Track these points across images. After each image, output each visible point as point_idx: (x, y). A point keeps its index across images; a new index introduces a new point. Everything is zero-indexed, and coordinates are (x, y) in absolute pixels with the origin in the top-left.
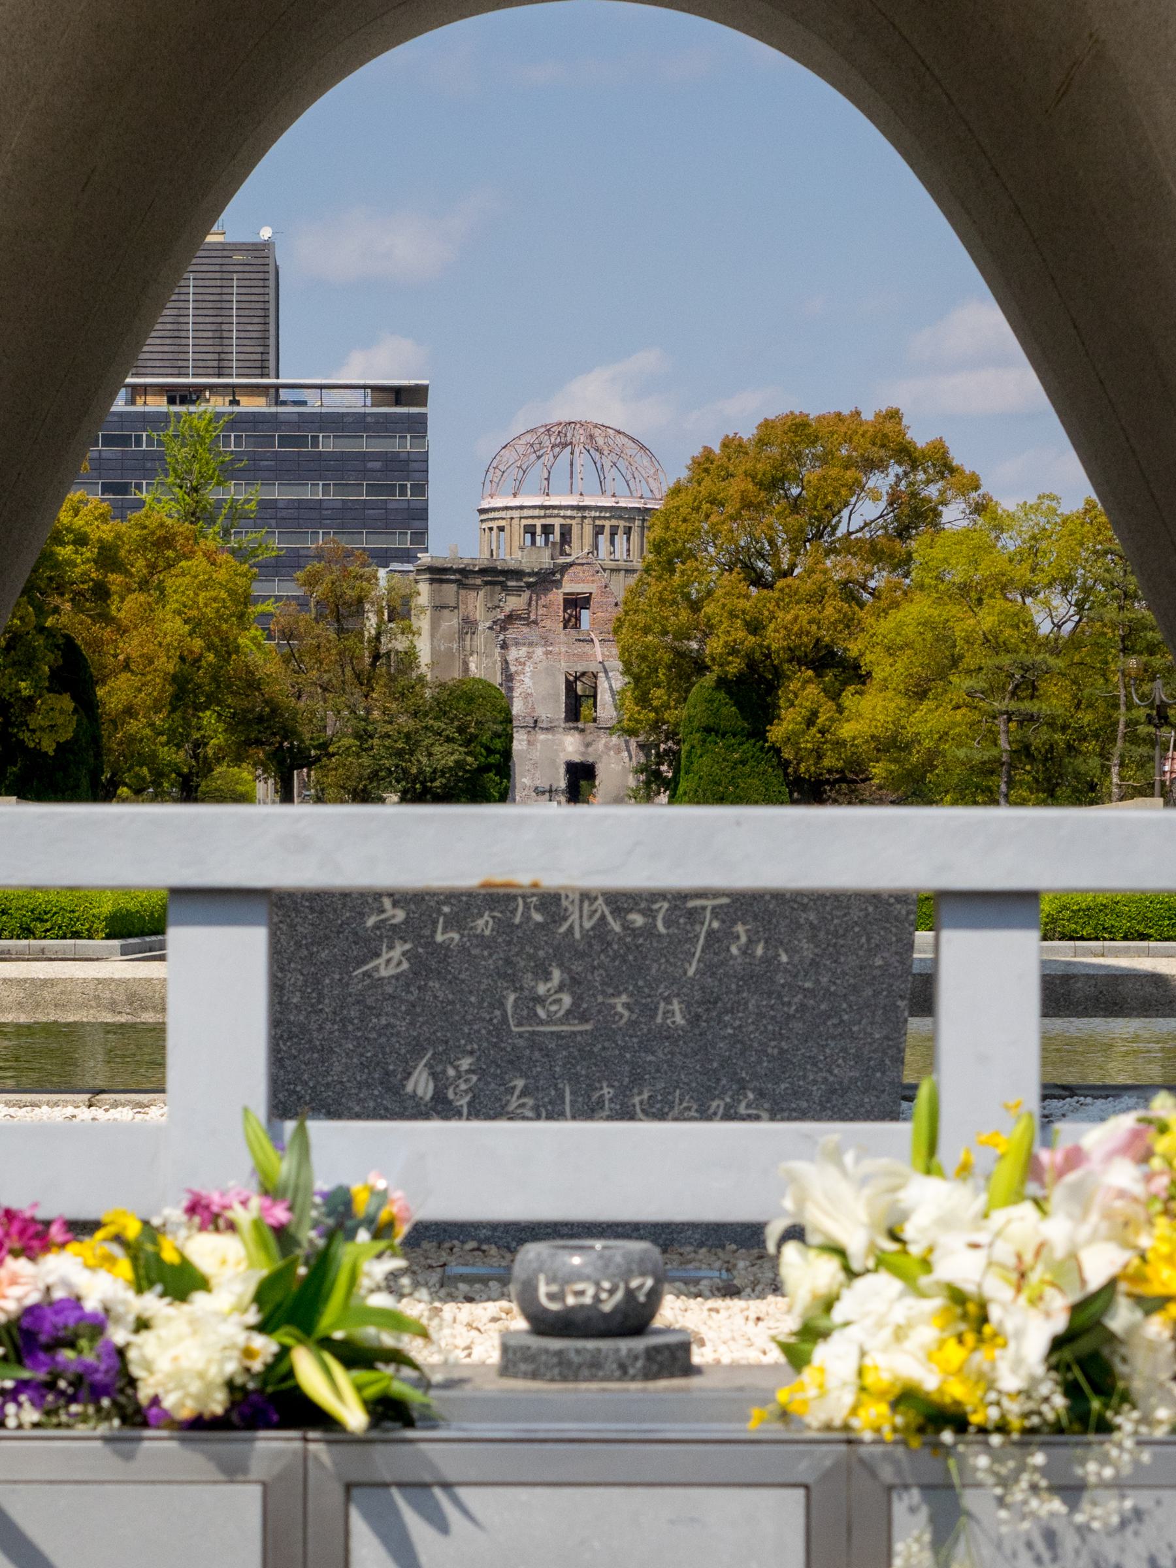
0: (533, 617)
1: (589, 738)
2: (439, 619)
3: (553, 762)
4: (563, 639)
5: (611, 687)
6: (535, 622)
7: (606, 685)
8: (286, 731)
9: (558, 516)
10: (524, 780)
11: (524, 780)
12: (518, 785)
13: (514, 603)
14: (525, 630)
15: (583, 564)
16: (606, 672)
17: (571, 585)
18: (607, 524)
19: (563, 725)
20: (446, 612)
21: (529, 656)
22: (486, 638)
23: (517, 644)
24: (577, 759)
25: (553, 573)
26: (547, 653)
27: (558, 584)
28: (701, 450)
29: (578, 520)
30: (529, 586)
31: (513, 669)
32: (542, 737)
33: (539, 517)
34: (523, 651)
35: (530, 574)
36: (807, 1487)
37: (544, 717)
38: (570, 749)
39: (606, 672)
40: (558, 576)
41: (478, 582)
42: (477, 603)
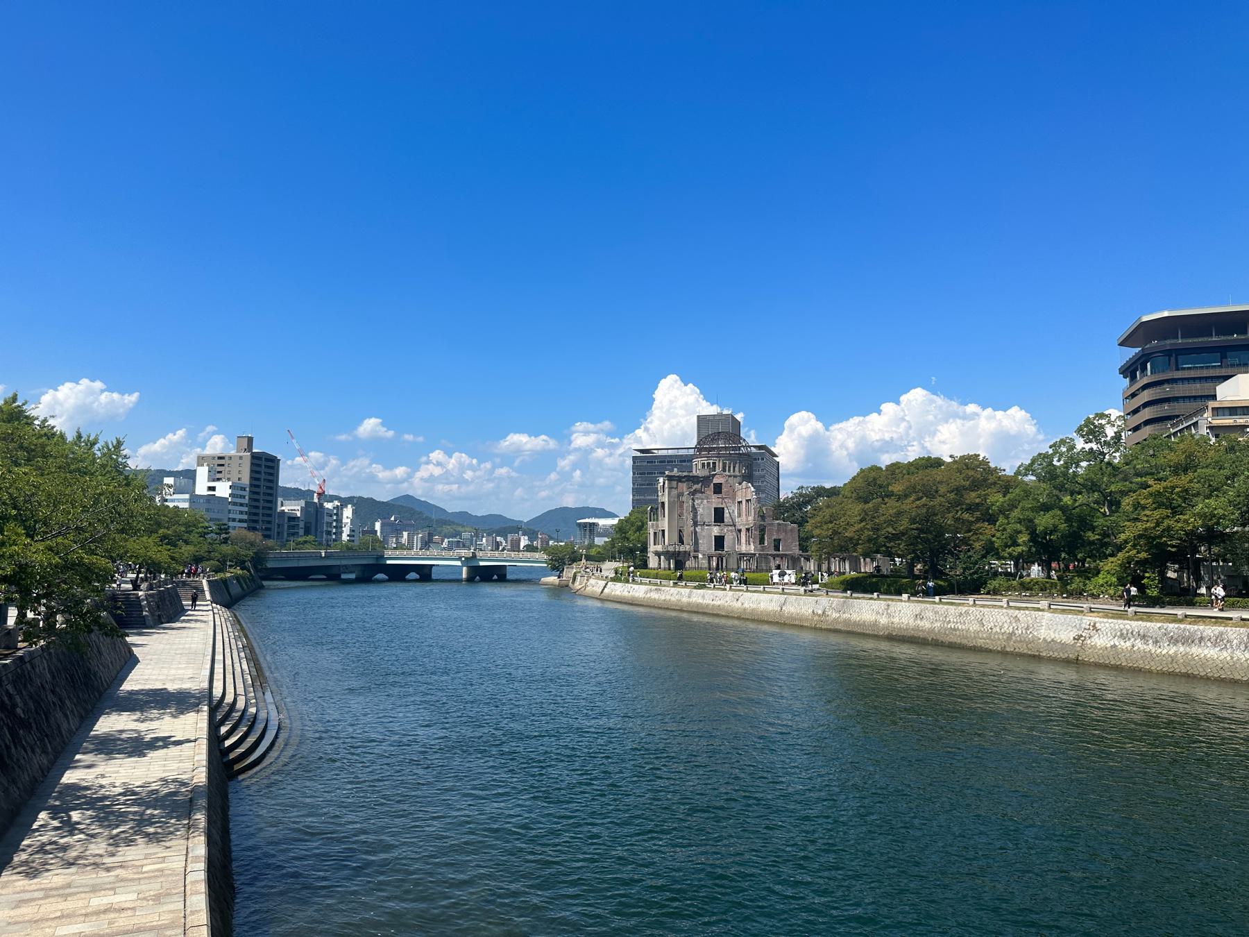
13: (698, 486)
42: (683, 487)
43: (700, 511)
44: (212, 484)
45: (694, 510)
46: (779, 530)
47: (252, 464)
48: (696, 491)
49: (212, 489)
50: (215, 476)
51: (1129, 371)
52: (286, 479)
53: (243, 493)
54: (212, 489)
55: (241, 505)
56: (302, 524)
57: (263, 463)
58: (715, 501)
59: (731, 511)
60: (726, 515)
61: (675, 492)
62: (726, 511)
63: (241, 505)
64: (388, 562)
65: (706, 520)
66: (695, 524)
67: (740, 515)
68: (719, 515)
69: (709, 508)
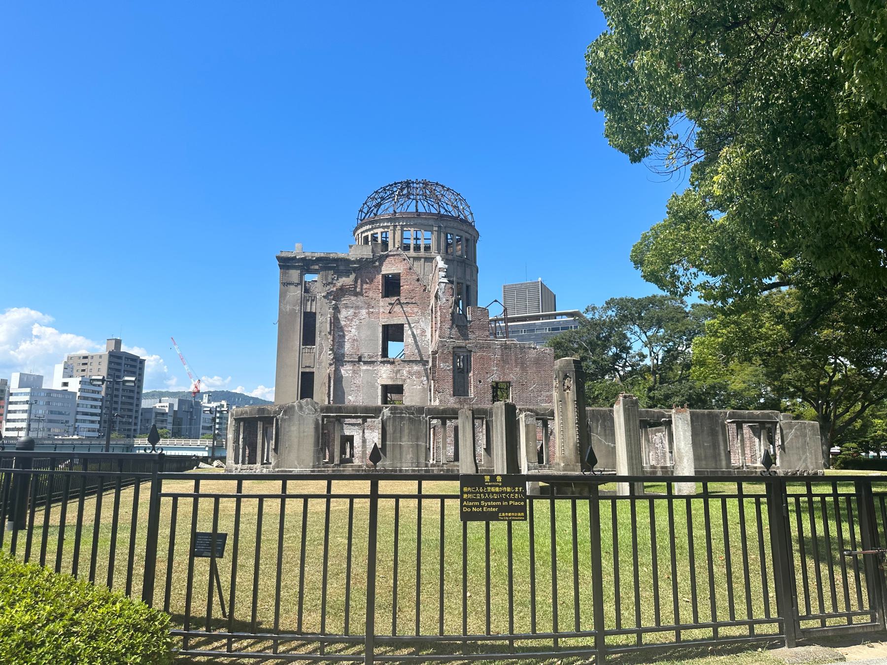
0: (358, 290)
1: (398, 367)
2: (286, 291)
3: (373, 386)
4: (383, 304)
5: (413, 333)
6: (361, 294)
7: (410, 332)
8: (867, 51)
10: (350, 397)
11: (350, 397)
13: (346, 281)
14: (353, 298)
15: (393, 255)
16: (409, 324)
17: (389, 268)
18: (369, 233)
19: (380, 359)
20: (292, 287)
22: (322, 305)
23: (346, 307)
24: (390, 382)
26: (368, 313)
27: (378, 269)
29: (391, 228)
30: (355, 270)
31: (343, 323)
32: (364, 367)
33: (369, 230)
34: (351, 312)
35: (354, 262)
36: (496, 301)
37: (366, 355)
38: (384, 376)
39: (409, 324)
40: (377, 263)
41: (317, 267)
43: (351, 333)
44: (66, 380)
45: (336, 328)
48: (342, 292)
49: (65, 384)
50: (68, 371)
55: (95, 400)
56: (170, 420)
58: (384, 312)
63: (95, 400)
65: (366, 353)
66: (339, 360)
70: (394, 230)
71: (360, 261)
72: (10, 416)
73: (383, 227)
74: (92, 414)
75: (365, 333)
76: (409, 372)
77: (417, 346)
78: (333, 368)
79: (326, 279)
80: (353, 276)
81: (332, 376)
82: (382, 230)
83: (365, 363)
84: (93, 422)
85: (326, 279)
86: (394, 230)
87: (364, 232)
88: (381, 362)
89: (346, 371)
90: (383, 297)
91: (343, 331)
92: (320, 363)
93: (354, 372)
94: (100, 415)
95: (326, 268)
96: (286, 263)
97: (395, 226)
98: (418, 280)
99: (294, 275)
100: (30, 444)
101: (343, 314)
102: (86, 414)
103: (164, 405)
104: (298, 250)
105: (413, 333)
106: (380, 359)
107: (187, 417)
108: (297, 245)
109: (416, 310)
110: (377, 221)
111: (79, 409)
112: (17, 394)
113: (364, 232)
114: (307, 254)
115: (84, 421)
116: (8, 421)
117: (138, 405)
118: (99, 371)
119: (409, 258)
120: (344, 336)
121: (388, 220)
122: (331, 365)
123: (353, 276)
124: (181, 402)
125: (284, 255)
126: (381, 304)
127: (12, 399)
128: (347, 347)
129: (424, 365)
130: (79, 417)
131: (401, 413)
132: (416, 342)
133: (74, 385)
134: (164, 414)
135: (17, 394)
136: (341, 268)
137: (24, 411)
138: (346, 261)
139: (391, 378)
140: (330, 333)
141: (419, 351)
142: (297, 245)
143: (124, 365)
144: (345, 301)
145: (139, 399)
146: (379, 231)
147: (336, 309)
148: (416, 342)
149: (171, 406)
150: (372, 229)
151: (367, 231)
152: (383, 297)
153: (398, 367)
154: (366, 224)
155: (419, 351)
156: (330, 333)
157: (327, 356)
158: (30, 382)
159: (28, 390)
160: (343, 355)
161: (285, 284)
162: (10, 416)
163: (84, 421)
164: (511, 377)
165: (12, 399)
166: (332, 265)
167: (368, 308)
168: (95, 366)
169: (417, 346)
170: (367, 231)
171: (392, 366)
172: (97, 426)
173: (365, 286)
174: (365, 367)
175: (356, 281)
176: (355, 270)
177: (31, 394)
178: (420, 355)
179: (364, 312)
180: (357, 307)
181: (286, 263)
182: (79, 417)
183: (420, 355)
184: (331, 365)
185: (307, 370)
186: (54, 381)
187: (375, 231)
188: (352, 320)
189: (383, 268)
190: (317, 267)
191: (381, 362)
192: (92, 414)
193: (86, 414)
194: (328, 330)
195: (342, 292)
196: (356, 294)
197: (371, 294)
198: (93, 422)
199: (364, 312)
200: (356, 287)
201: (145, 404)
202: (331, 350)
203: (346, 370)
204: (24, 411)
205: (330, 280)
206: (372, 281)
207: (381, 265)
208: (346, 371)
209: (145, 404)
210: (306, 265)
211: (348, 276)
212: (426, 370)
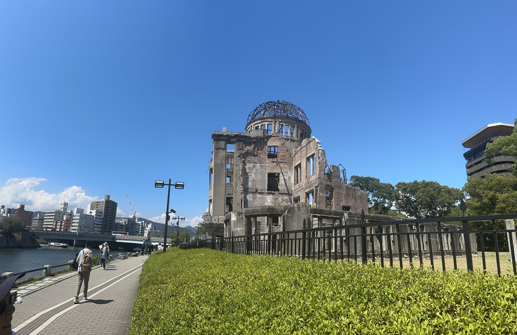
0: (256, 153)
5: (284, 178)
6: (257, 155)
7: (283, 178)
9: (266, 121)
12: (245, 226)
13: (250, 148)
14: (253, 158)
15: (275, 136)
16: (282, 173)
18: (260, 125)
19: (266, 192)
20: (221, 150)
21: (254, 167)
22: (237, 160)
23: (249, 162)
25: (264, 139)
26: (261, 166)
28: (422, 181)
29: (273, 122)
30: (254, 142)
31: (247, 171)
33: (260, 123)
34: (252, 165)
35: (253, 138)
37: (259, 189)
38: (269, 201)
39: (282, 173)
40: (266, 140)
41: (234, 140)
42: (231, 148)
43: (252, 176)
44: (91, 211)
45: (245, 175)
46: (347, 195)
47: (106, 204)
48: (247, 154)
49: (91, 213)
50: (92, 208)
51: (467, 156)
52: (119, 212)
53: (101, 214)
54: (91, 213)
55: (100, 219)
56: (125, 228)
57: (110, 204)
58: (270, 166)
59: (287, 178)
60: (282, 182)
61: (222, 153)
62: (281, 178)
63: (100, 219)
64: (117, 241)
65: (259, 187)
66: (246, 191)
67: (297, 181)
68: (273, 181)
69: (263, 174)
70: (275, 123)
71: (257, 138)
72: (73, 224)
73: (269, 121)
74: (99, 225)
75: (259, 177)
76: (282, 199)
77: (286, 185)
78: (243, 195)
79: (239, 147)
80: (253, 146)
81: (243, 200)
82: (268, 123)
83: (259, 193)
84: (99, 228)
85: (239, 147)
86: (275, 123)
87: (256, 124)
88: (267, 193)
89: (249, 197)
90: (268, 158)
91: (247, 175)
92: (236, 193)
93: (254, 198)
94: (101, 225)
95: (238, 141)
96: (217, 138)
97: (276, 121)
98: (287, 151)
99: (222, 144)
100: (80, 235)
101: (248, 166)
102: (97, 224)
103: (122, 222)
104: (224, 131)
105: (284, 178)
106: (266, 192)
107: (131, 227)
108: (223, 128)
109: (286, 166)
110: (265, 118)
111: (95, 222)
112: (76, 216)
113: (256, 124)
114: (229, 133)
115: (96, 227)
116: (72, 226)
117: (114, 221)
118: (102, 208)
119: (283, 139)
120: (248, 178)
121: (271, 118)
122: (242, 193)
123: (253, 146)
124: (127, 220)
125: (216, 133)
126: (267, 161)
127: (74, 218)
128: (250, 183)
129: (289, 196)
130: (95, 226)
131: (354, 217)
132: (286, 183)
133: (94, 213)
134: (123, 225)
135: (76, 216)
136: (247, 141)
137: (77, 223)
138: (249, 138)
139: (272, 202)
140: (242, 176)
141: (287, 188)
142: (223, 128)
143: (111, 206)
144: (248, 159)
145: (115, 219)
146: (266, 123)
147: (244, 163)
148: (286, 183)
149: (125, 222)
150: (262, 122)
151: (258, 123)
152: (268, 158)
153: (277, 197)
154: (258, 120)
155: (287, 188)
156: (242, 176)
157: (240, 189)
158: (80, 211)
159: (79, 214)
160: (248, 188)
161: (217, 149)
162: (73, 224)
163: (96, 227)
164: (350, 204)
165: (74, 218)
166: (241, 139)
167: (260, 163)
168: (101, 206)
169: (286, 185)
170: (258, 123)
171: (273, 196)
172: (100, 229)
173: (259, 152)
174: (259, 196)
175: (254, 149)
176: (254, 142)
177: (80, 216)
178: (288, 190)
179: (258, 165)
180: (255, 163)
181: (217, 138)
182: (95, 226)
183: (288, 190)
184: (242, 193)
185: (230, 196)
186: (87, 212)
187: (264, 123)
188: (252, 170)
189: (268, 143)
190: (234, 140)
191: (267, 193)
192: (99, 225)
193: (97, 224)
194: (241, 174)
195: (247, 154)
196: (254, 156)
197: (262, 156)
198: (99, 228)
199: (258, 165)
200: (254, 152)
201: (117, 221)
202: (242, 185)
203: (250, 197)
204: (77, 223)
205: (241, 147)
206: (262, 149)
207: (267, 141)
208: (249, 197)
209: (117, 221)
210: (229, 139)
211: (250, 146)
212: (290, 199)
